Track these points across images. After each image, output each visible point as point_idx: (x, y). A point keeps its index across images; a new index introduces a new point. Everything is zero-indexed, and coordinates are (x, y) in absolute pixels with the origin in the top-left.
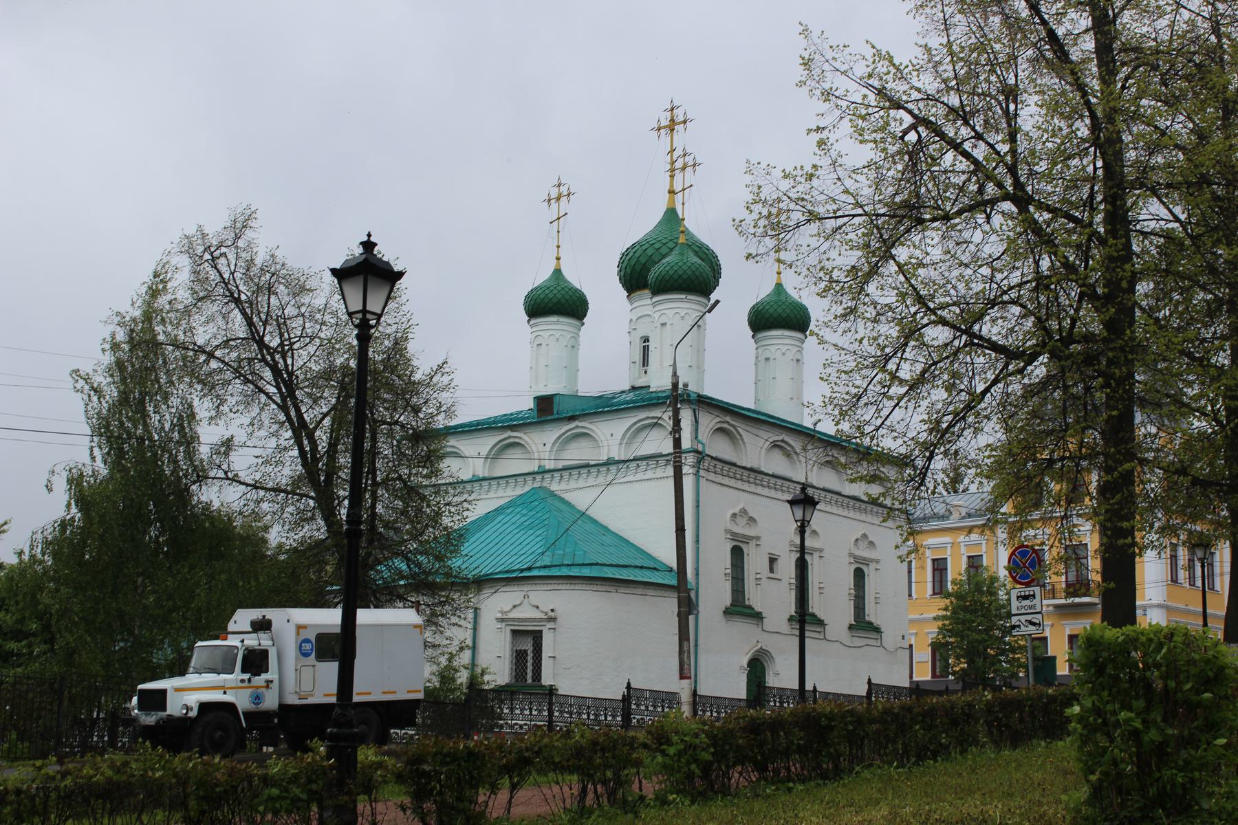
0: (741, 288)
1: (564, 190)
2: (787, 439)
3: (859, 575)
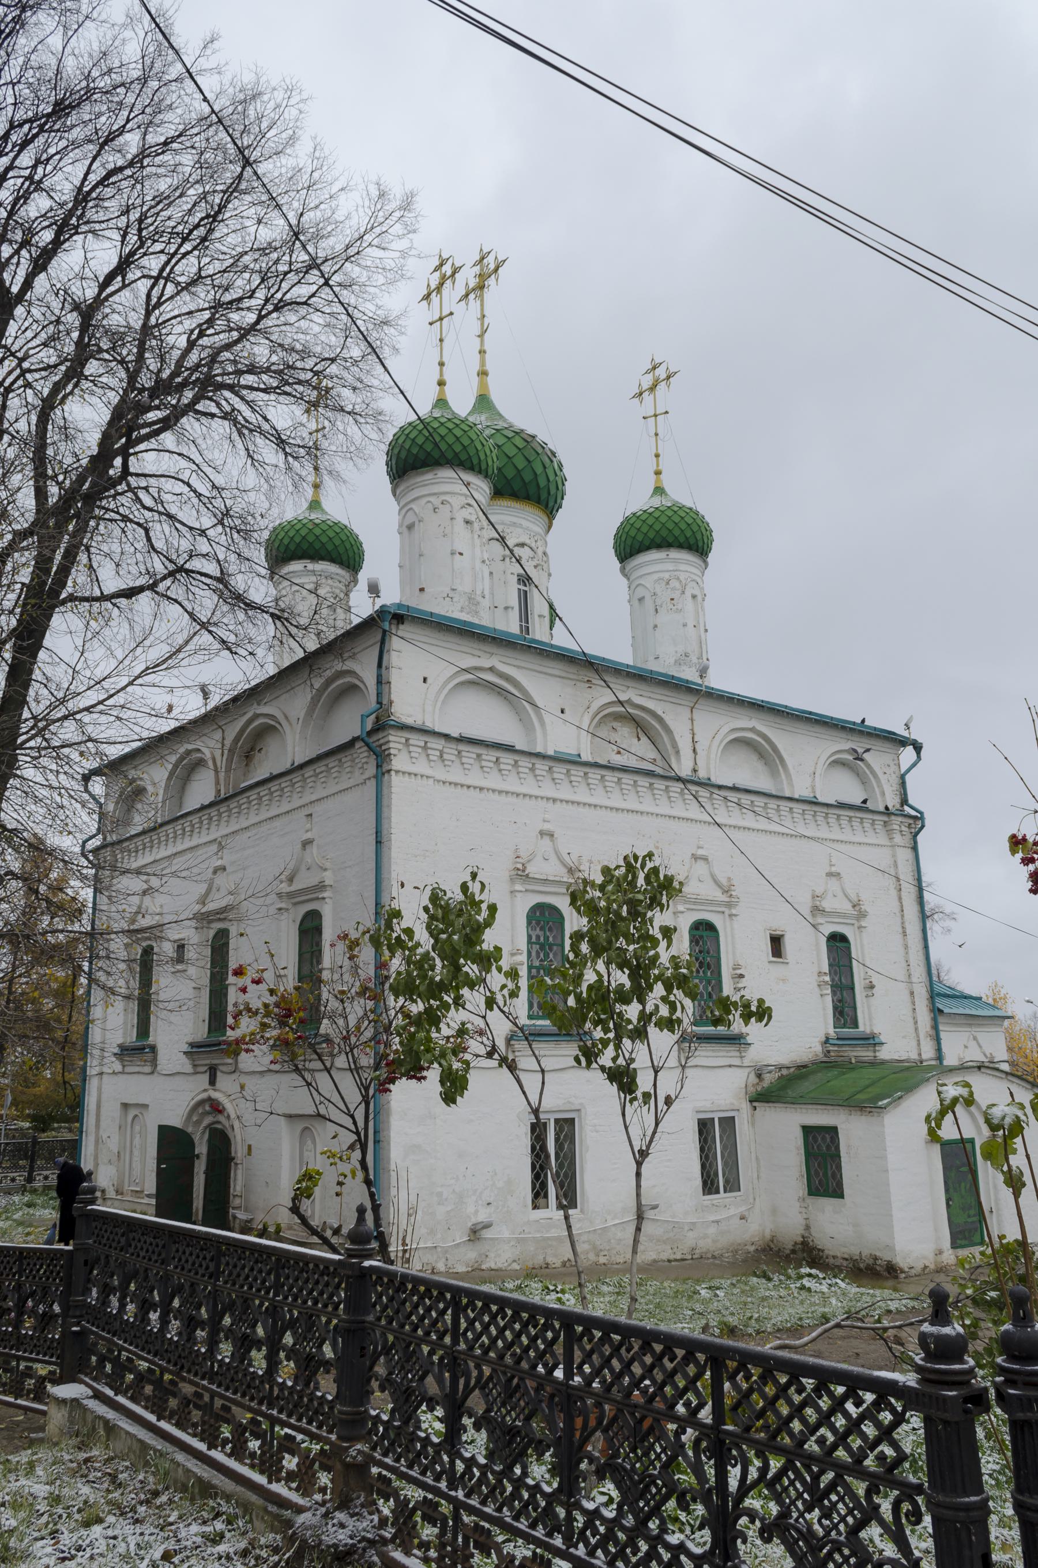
0: (597, 501)
3: (838, 942)
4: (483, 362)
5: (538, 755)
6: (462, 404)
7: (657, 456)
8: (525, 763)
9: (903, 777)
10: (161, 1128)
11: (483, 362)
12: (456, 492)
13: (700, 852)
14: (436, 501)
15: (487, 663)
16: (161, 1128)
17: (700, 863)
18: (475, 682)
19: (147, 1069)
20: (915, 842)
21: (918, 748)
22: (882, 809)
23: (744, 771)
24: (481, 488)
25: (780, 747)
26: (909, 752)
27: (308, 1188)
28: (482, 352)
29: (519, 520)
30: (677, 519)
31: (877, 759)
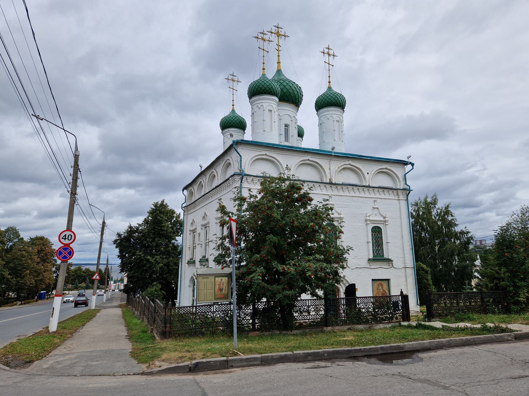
1: (326, 51)
2: (268, 153)
3: (377, 232)
4: (279, 59)
5: (364, 186)
6: (270, 75)
7: (329, 77)
8: (361, 188)
9: (405, 175)
10: (354, 285)
11: (279, 59)
12: (270, 102)
13: (375, 206)
14: (328, 116)
15: (384, 167)
16: (354, 285)
17: (376, 210)
18: (381, 172)
19: (371, 257)
20: (407, 198)
21: (413, 165)
22: (328, 181)
23: (352, 179)
24: (277, 99)
25: (323, 166)
26: (409, 167)
27: (92, 282)
28: (279, 56)
29: (288, 109)
30: (334, 97)
31: (398, 171)
